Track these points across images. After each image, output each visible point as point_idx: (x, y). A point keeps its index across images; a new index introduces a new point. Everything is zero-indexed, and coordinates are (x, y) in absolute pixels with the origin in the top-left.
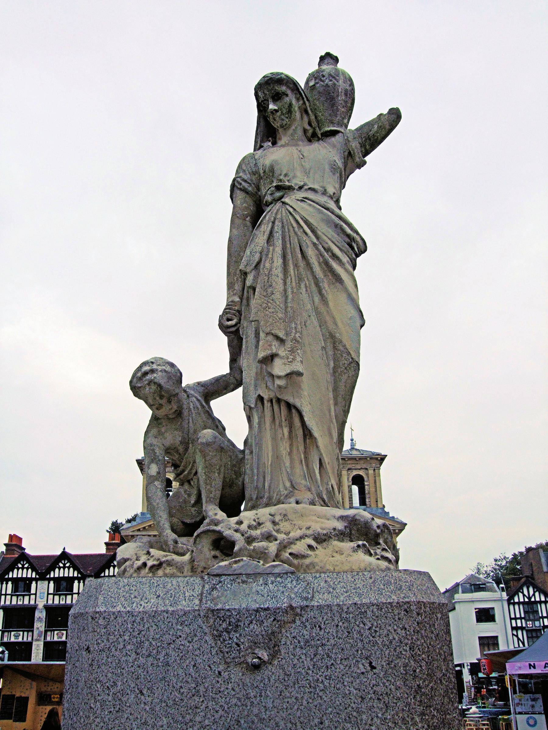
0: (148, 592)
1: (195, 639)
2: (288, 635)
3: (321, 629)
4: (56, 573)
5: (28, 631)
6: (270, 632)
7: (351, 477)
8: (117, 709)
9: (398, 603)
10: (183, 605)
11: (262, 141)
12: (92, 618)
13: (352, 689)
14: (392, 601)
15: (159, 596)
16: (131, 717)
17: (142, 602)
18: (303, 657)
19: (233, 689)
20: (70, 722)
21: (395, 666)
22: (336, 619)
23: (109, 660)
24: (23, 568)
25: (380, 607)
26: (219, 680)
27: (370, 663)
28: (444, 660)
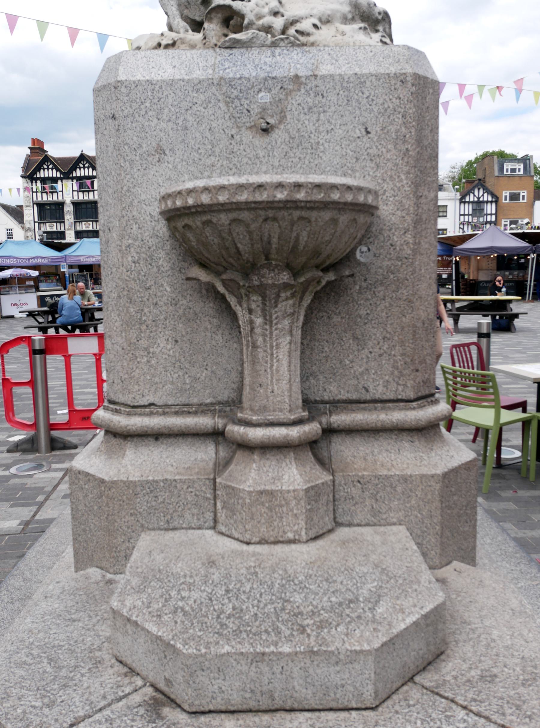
0: (164, 64)
1: (210, 105)
2: (294, 102)
3: (323, 97)
4: (79, 173)
5: (60, 222)
6: (277, 99)
8: (144, 167)
9: (395, 74)
10: (198, 74)
12: (115, 88)
13: (348, 151)
14: (389, 72)
15: (175, 67)
16: (157, 174)
17: (159, 72)
18: (307, 122)
19: (244, 150)
20: (104, 182)
21: (388, 132)
22: (337, 87)
23: (133, 125)
24: (48, 169)
25: (377, 77)
26: (233, 142)
27: (366, 129)
28: (431, 130)
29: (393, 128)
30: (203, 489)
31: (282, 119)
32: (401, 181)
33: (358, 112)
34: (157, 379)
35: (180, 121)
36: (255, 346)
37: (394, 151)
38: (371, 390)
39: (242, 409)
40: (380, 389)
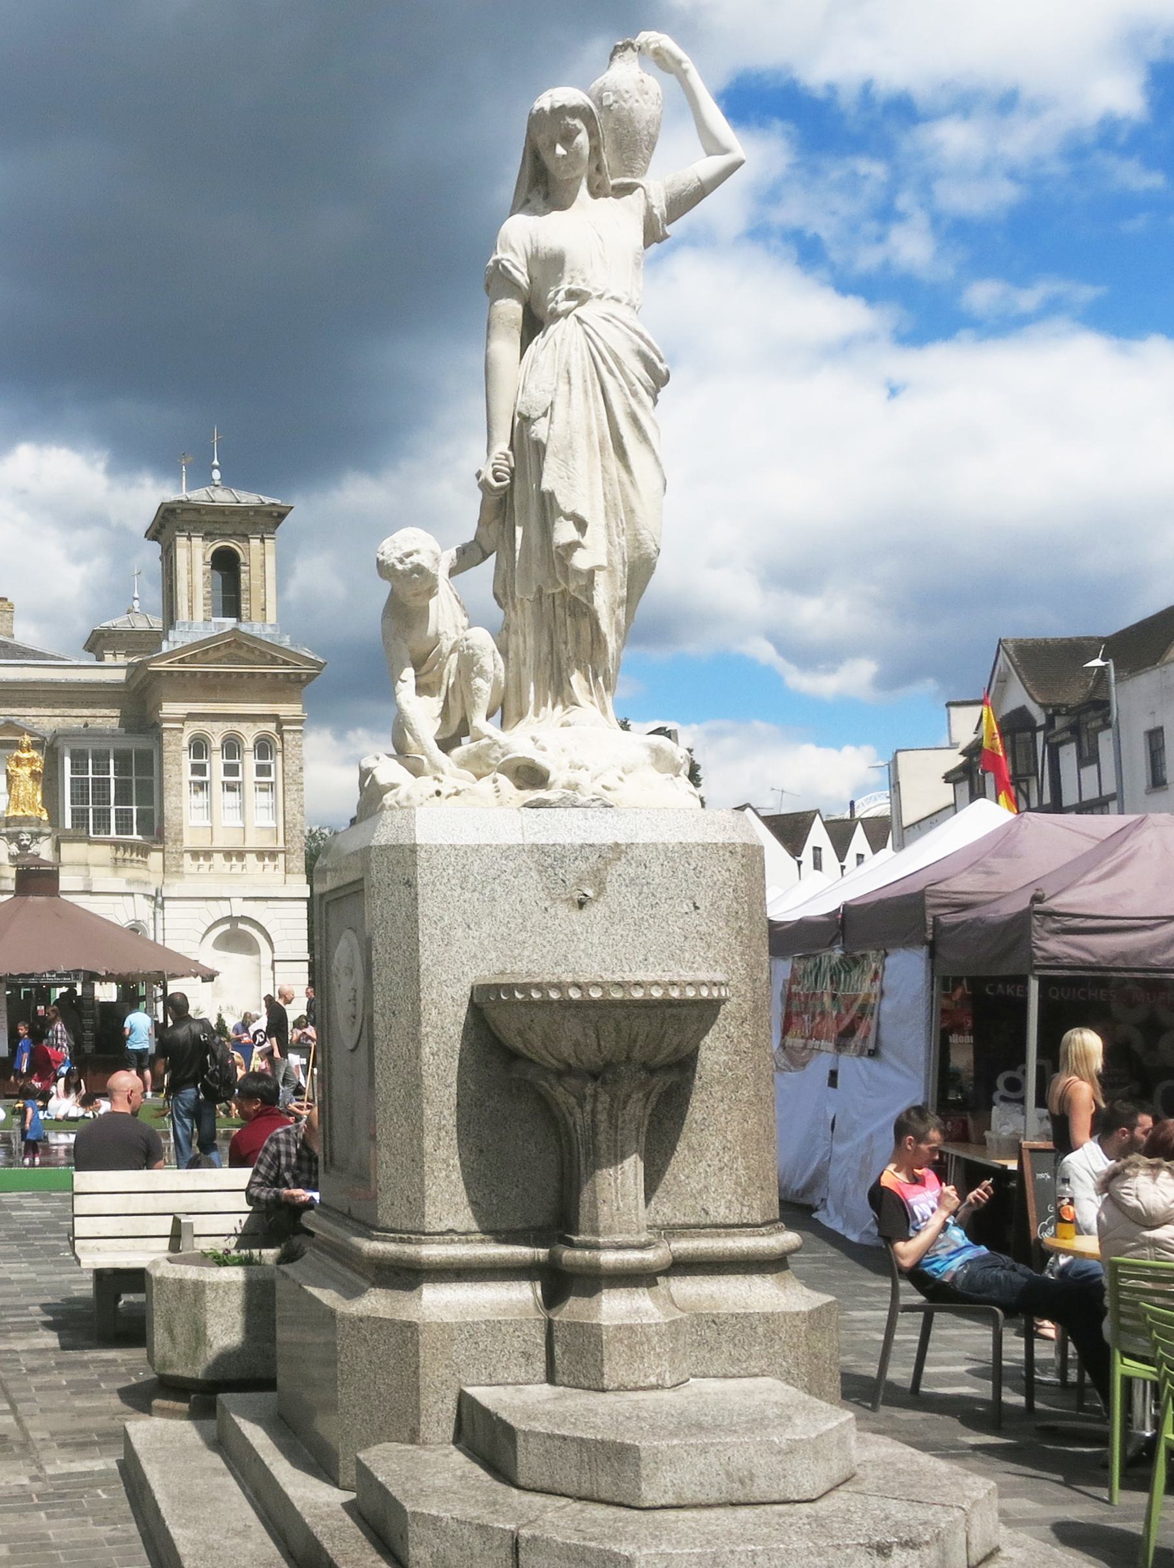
13: (676, 928)
25: (705, 847)
29: (723, 904)
30: (533, 1332)
31: (601, 891)
32: (735, 963)
33: (684, 884)
35: (487, 891)
37: (726, 929)
38: (711, 1212)
40: (723, 1211)
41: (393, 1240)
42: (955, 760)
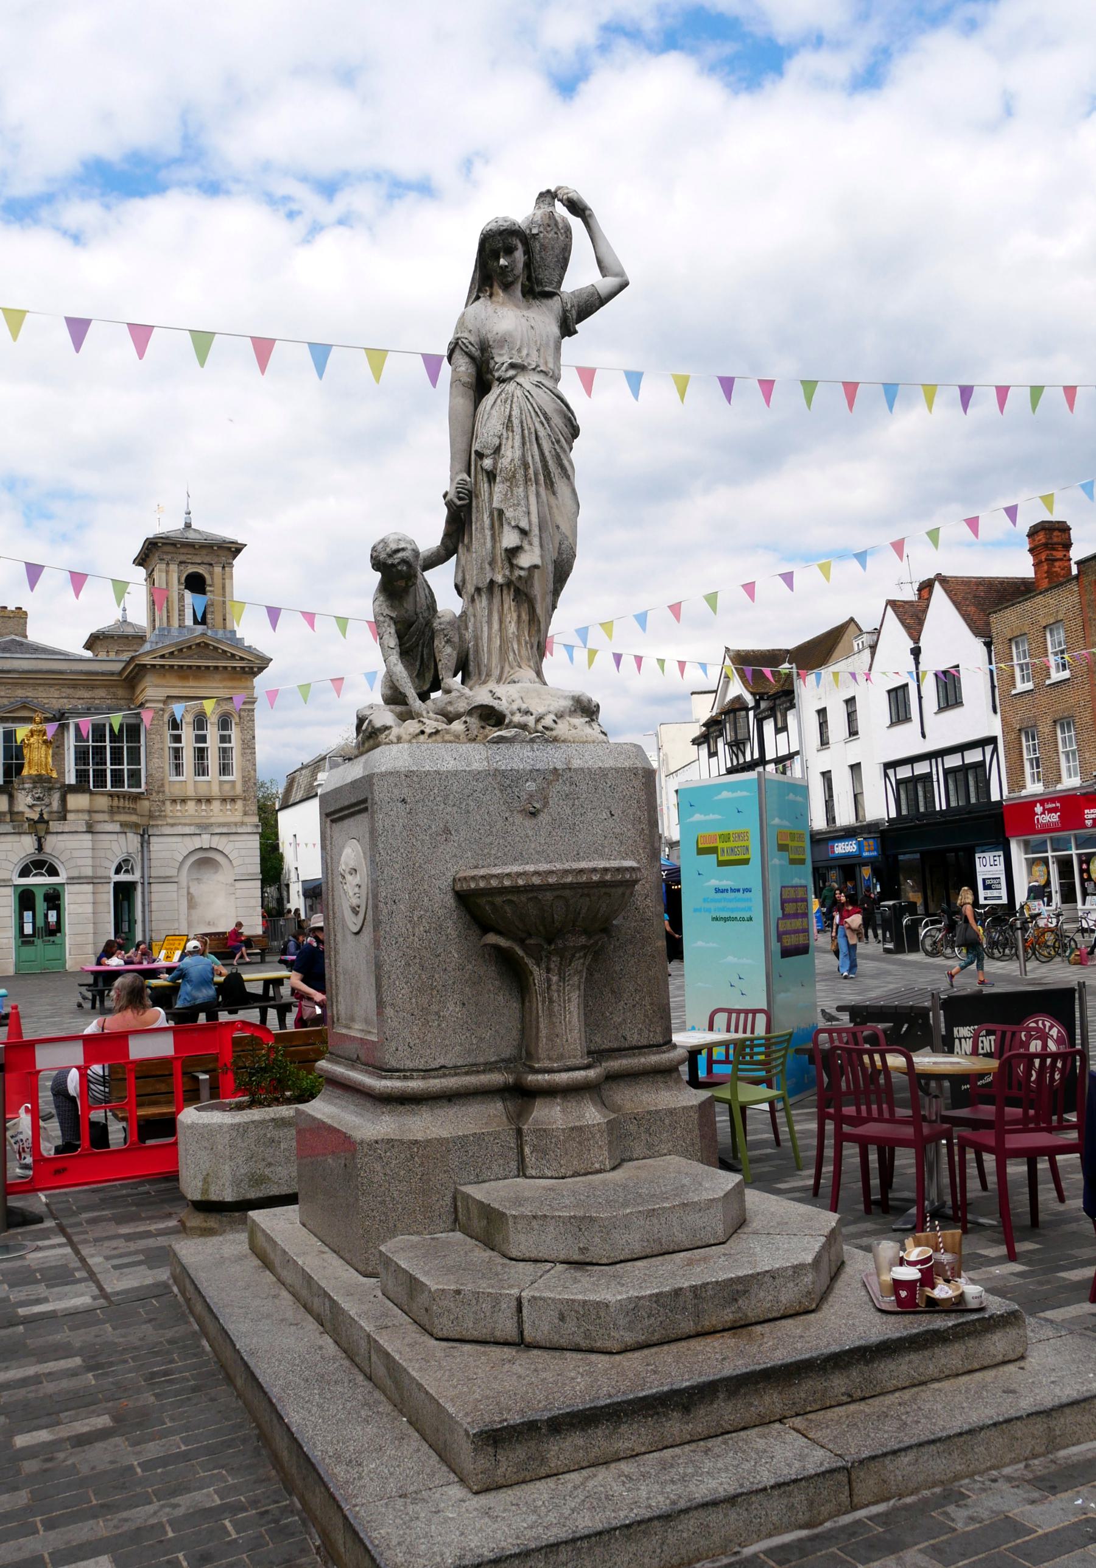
7: (185, 576)
10: (476, 766)
11: (480, 290)
25: (617, 770)
29: (630, 812)
31: (546, 804)
32: (640, 855)
34: (447, 1042)
35: (463, 806)
36: (551, 1001)
39: (538, 1060)
40: (636, 1036)
41: (399, 1078)
42: (697, 730)
